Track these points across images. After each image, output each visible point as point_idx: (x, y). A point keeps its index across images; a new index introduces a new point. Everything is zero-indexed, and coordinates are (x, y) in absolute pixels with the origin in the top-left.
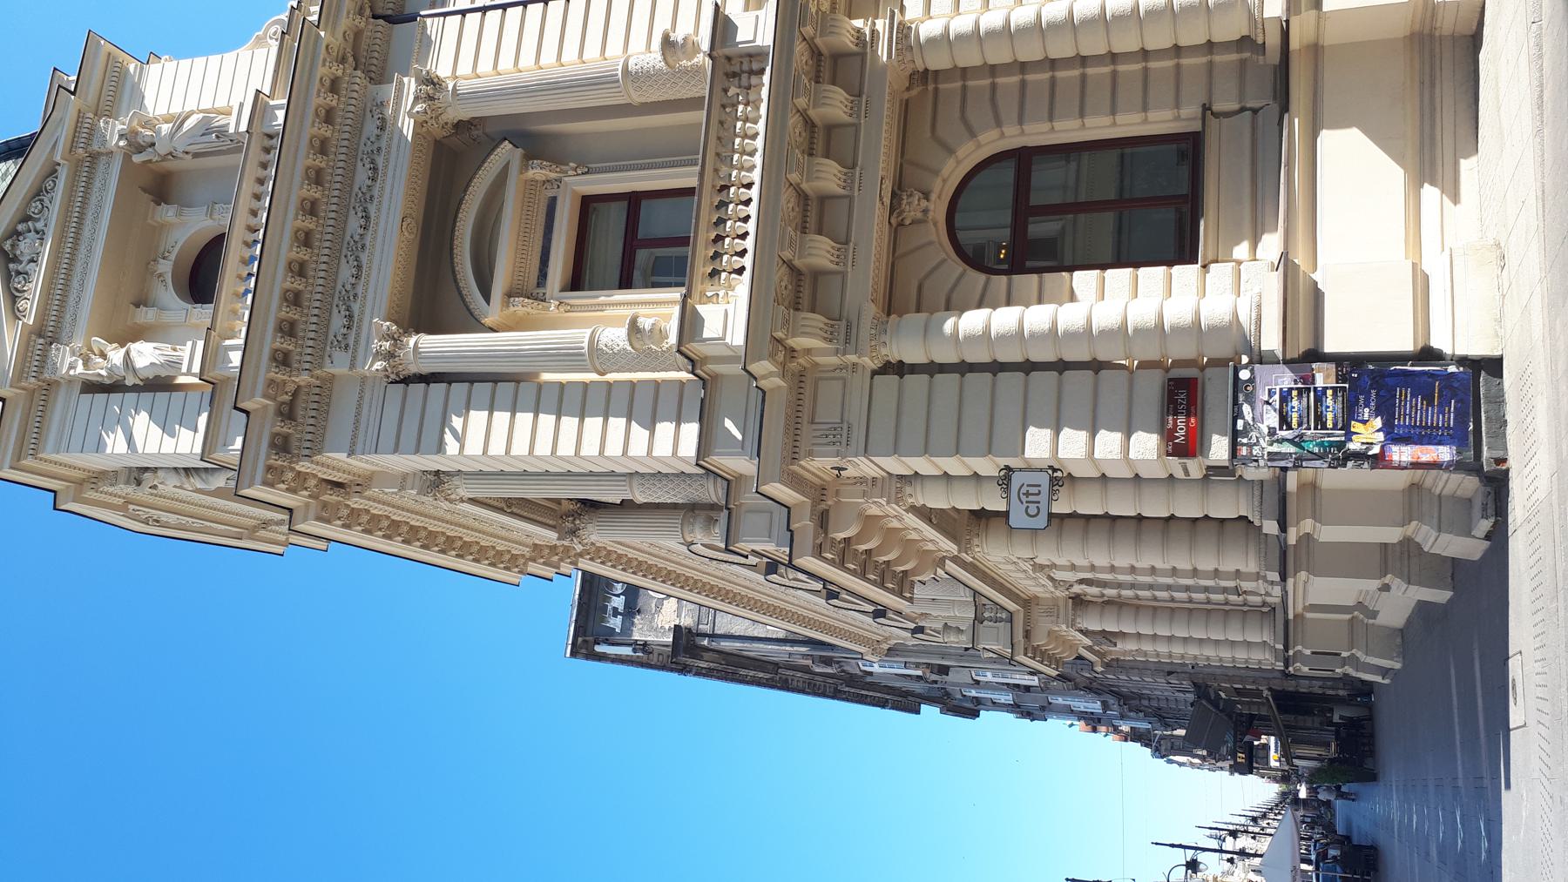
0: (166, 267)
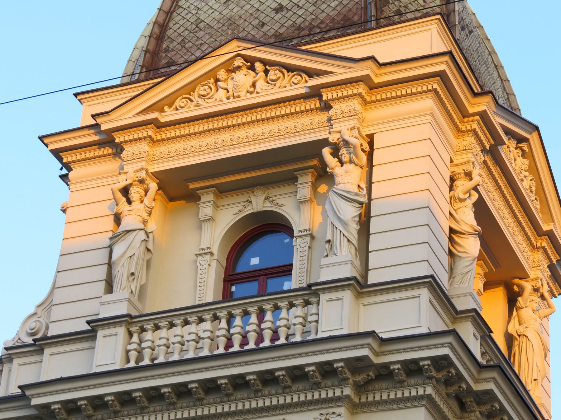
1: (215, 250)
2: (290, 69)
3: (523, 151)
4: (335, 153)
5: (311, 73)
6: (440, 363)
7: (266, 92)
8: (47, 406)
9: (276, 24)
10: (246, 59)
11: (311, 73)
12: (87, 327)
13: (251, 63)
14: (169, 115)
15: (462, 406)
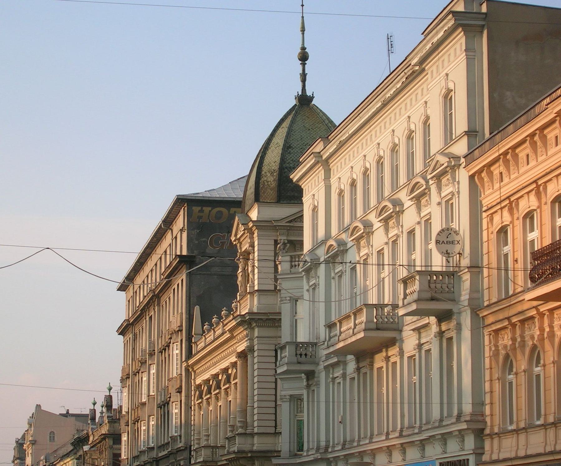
14: (238, 236)
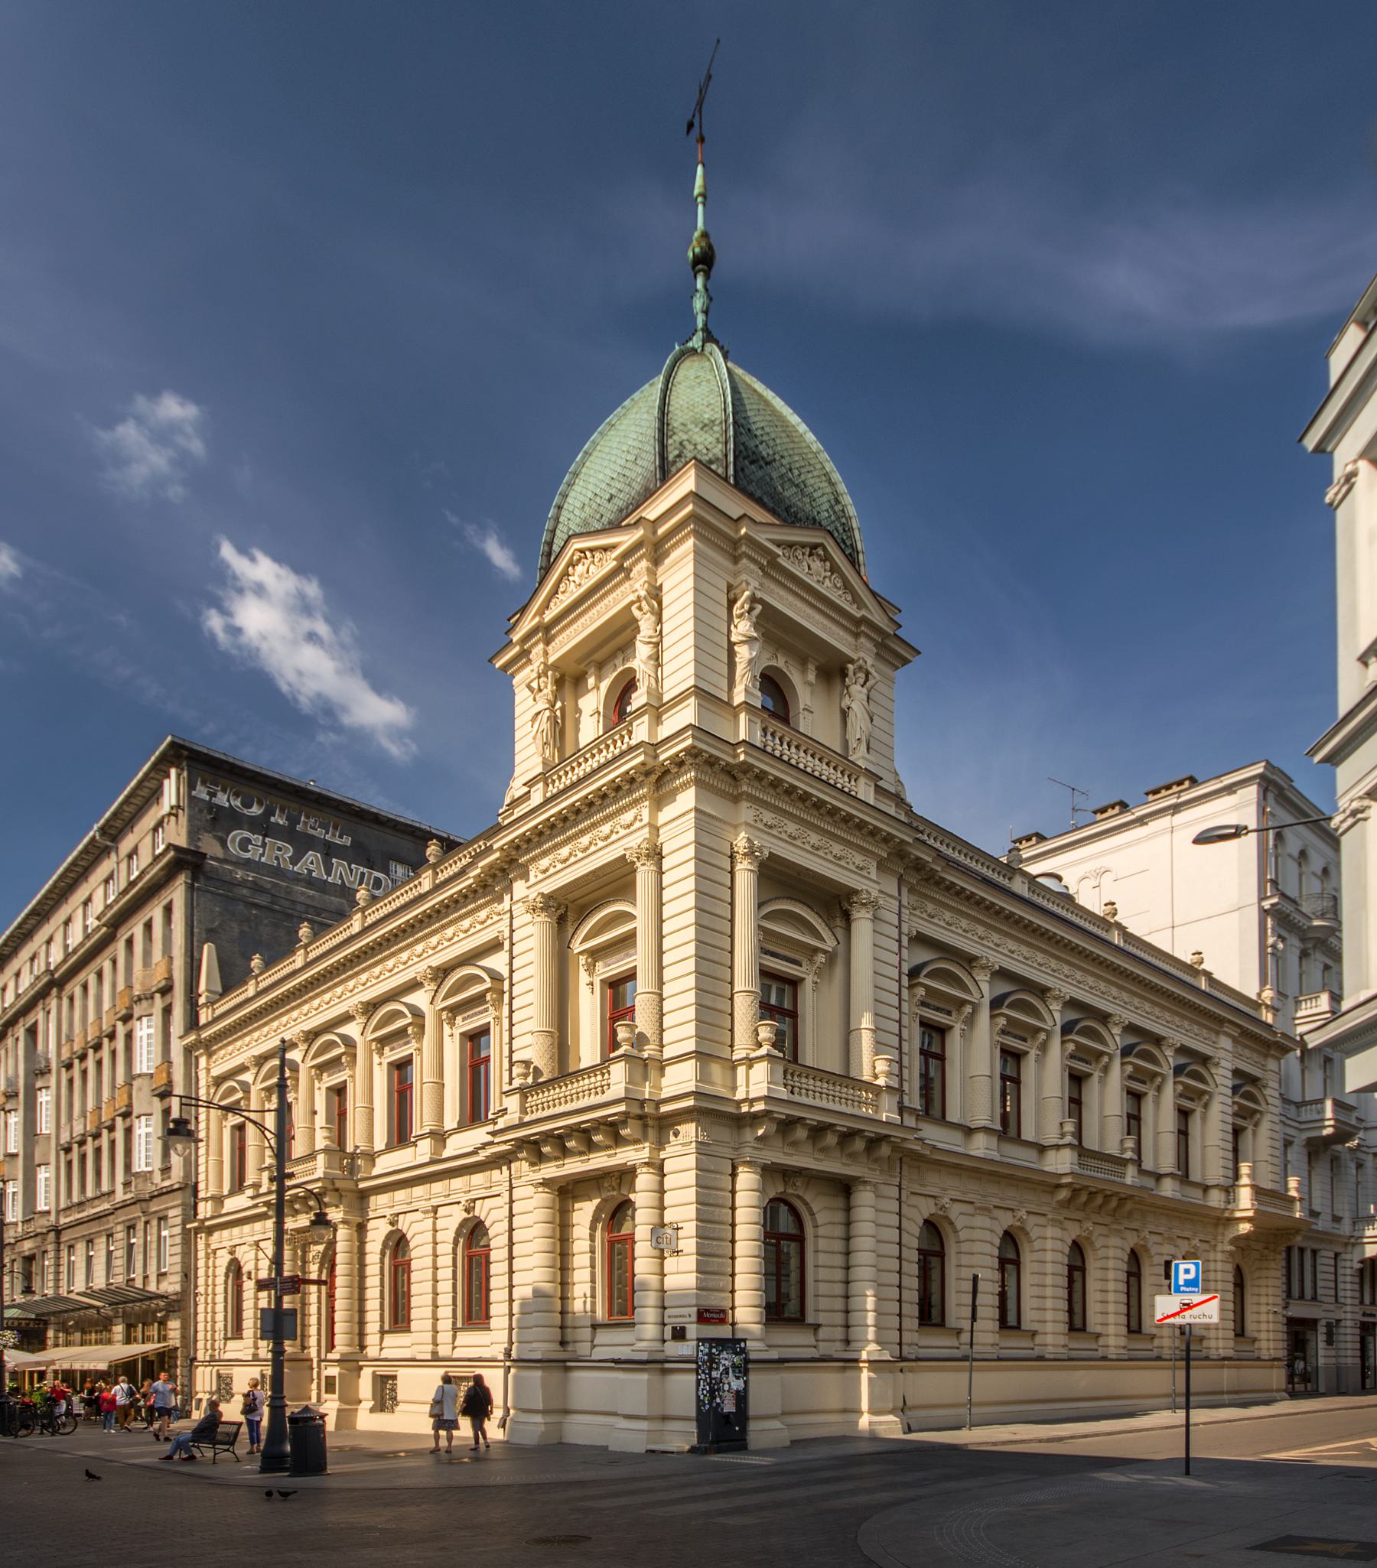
0: (780, 663)
1: (601, 710)
2: (606, 549)
3: (819, 556)
4: (640, 609)
5: (614, 547)
6: (693, 752)
7: (597, 573)
8: (501, 849)
9: (609, 513)
10: (582, 551)
11: (614, 547)
12: (526, 789)
13: (827, 558)
14: (548, 616)
15: (734, 778)
